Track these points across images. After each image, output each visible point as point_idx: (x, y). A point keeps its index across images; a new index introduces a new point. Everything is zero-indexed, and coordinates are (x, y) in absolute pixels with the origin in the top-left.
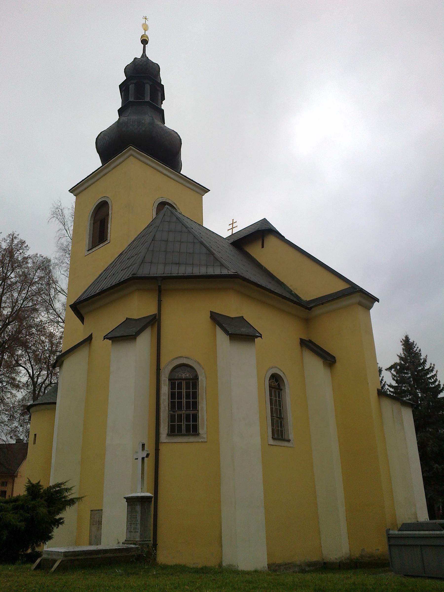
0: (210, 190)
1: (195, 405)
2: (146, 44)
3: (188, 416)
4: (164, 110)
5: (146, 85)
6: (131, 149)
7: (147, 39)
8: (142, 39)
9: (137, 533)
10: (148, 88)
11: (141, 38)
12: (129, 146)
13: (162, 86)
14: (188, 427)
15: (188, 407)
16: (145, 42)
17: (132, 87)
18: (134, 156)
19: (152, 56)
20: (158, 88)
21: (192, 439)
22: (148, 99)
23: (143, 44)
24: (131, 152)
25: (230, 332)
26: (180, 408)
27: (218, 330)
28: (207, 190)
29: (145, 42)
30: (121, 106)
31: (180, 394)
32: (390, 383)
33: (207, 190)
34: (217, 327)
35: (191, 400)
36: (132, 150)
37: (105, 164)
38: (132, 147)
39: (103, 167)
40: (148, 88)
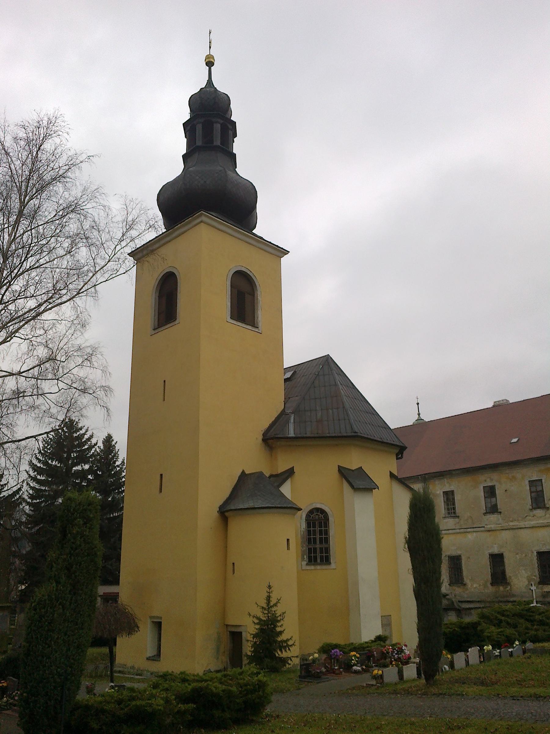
0: (289, 252)
1: (327, 540)
2: (212, 66)
3: (321, 549)
4: (236, 154)
5: (215, 125)
6: (202, 214)
7: (212, 60)
8: (207, 61)
9: (499, 492)
10: (217, 127)
11: (205, 60)
12: (200, 211)
13: (234, 123)
14: (322, 558)
15: (321, 542)
16: (210, 64)
17: (199, 128)
18: (205, 223)
19: (220, 86)
20: (230, 127)
21: (324, 567)
22: (217, 142)
23: (208, 66)
24: (203, 218)
25: (355, 487)
26: (315, 542)
27: (345, 484)
28: (286, 252)
29: (210, 64)
30: (185, 152)
31: (314, 531)
32: (500, 512)
33: (286, 252)
34: (344, 480)
35: (323, 536)
36: (205, 217)
37: (169, 230)
38: (203, 212)
39: (167, 233)
40: (217, 127)
